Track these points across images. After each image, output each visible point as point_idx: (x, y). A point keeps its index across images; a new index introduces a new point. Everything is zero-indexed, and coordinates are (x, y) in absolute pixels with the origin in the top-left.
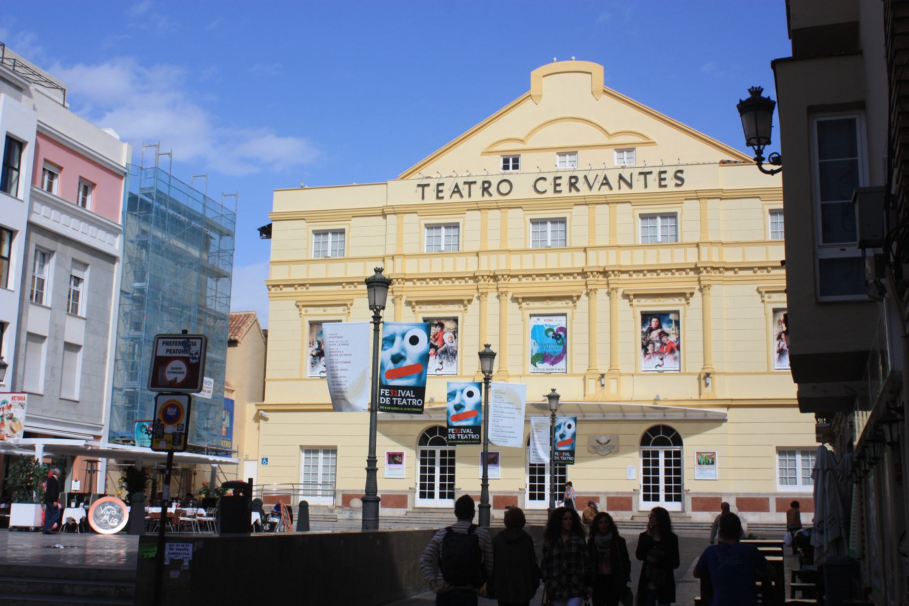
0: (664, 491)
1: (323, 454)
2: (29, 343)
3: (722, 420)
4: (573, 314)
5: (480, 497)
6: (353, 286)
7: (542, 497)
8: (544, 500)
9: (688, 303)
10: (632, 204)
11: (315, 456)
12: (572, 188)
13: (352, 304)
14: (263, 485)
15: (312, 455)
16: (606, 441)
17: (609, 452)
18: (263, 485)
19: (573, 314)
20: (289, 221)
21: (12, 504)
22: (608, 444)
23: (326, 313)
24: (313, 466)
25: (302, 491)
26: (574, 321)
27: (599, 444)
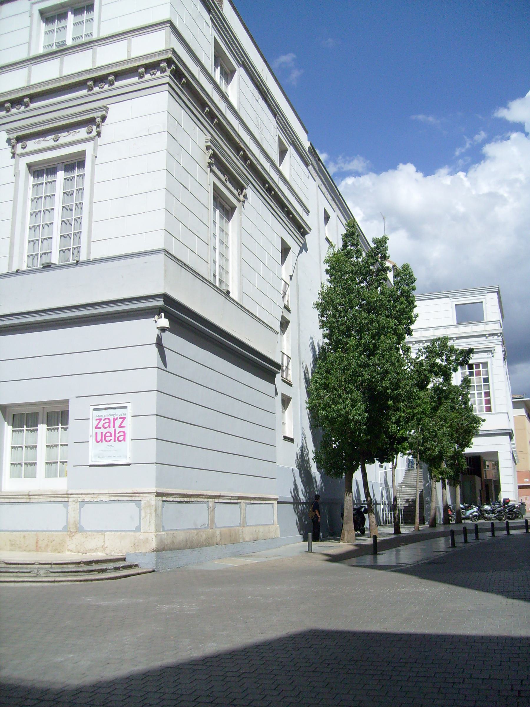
1: (63, 172)
2: (485, 320)
4: (492, 362)
5: (506, 528)
6: (491, 353)
11: (50, 178)
13: (104, 118)
15: (44, 179)
19: (492, 362)
20: (19, 121)
21: (292, 505)
23: (58, 143)
24: (61, 445)
26: (97, 161)
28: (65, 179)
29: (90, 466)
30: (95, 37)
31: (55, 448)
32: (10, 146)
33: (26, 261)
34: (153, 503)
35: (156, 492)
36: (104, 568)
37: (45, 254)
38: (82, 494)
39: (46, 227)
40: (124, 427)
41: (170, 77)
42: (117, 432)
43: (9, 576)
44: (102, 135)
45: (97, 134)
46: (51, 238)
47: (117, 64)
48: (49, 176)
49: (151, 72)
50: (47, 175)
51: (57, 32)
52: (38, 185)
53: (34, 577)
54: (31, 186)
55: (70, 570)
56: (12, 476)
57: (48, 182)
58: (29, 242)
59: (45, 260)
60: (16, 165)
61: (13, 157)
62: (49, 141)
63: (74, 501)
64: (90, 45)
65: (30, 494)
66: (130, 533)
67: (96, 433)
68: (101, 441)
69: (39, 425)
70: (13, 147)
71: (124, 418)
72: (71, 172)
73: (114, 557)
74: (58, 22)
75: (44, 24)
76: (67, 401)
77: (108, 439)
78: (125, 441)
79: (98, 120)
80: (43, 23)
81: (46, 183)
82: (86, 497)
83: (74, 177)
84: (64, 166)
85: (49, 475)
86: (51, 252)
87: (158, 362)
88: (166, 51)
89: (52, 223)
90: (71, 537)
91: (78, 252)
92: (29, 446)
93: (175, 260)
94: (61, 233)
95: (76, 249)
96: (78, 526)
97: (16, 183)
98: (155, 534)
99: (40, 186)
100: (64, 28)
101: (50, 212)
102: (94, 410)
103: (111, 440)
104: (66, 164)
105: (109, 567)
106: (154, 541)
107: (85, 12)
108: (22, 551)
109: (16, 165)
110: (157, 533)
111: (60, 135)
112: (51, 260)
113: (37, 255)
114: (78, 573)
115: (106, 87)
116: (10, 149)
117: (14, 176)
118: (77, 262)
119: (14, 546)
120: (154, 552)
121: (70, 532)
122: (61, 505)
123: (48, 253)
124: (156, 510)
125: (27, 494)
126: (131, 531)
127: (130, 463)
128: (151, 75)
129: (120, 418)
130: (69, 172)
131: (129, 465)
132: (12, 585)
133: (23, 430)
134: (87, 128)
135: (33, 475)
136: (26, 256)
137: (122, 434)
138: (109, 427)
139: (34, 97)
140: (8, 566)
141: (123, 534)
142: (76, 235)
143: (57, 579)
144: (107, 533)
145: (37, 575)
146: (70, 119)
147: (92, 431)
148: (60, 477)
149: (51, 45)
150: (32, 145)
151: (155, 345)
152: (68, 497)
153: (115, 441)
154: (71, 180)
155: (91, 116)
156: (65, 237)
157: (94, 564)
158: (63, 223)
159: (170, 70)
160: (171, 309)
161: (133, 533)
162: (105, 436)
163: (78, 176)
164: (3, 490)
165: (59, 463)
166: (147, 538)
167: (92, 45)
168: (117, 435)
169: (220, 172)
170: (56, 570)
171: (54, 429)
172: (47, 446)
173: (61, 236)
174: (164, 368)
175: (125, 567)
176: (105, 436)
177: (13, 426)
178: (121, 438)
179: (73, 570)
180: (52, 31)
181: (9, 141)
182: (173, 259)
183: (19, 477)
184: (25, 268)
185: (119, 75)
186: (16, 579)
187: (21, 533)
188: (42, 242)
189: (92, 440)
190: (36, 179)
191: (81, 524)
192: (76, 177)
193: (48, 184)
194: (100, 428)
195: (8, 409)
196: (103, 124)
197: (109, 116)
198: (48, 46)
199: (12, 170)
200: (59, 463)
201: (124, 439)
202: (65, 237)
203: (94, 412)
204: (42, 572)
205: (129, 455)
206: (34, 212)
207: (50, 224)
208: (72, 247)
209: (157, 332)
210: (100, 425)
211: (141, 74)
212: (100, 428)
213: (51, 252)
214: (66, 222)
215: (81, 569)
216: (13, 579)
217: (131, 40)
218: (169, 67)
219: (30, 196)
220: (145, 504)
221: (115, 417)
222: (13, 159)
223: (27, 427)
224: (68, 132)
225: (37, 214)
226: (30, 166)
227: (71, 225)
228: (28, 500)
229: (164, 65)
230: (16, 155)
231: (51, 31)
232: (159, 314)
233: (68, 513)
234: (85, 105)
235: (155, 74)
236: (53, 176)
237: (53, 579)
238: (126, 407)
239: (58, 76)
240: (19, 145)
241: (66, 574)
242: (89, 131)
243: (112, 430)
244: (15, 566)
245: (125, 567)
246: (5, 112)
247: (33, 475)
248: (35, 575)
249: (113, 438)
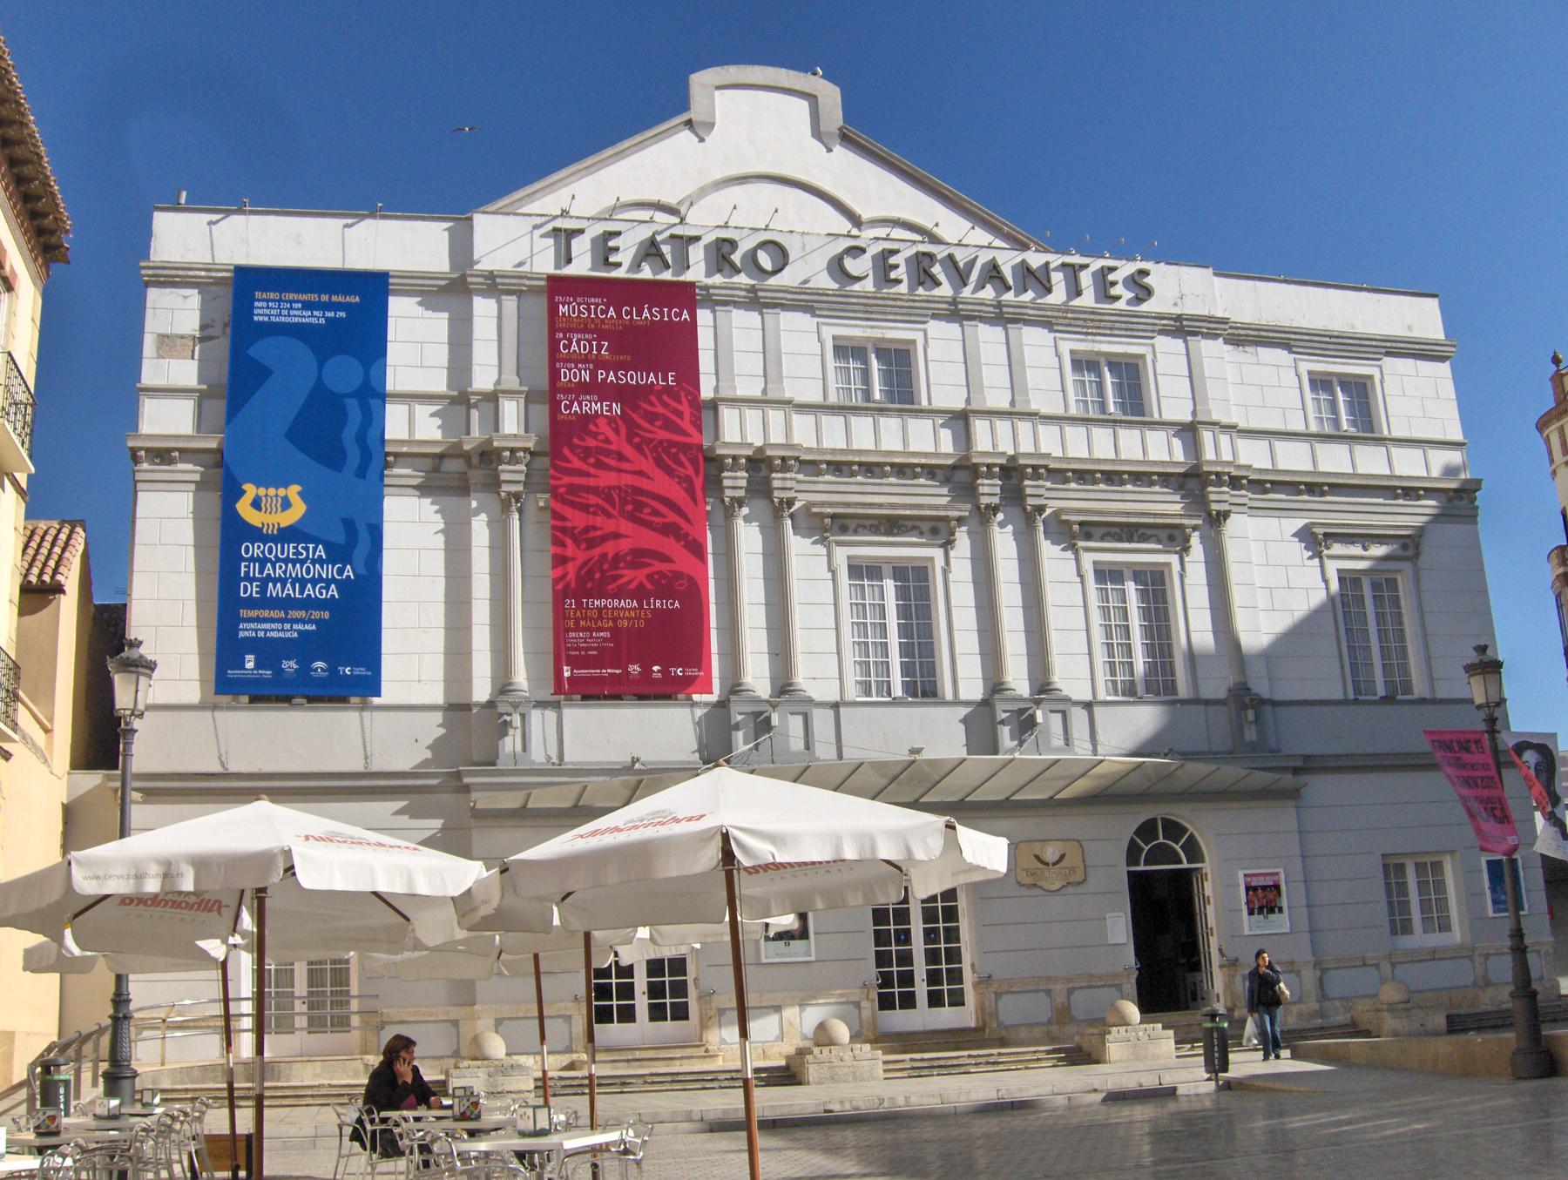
0: (646, 995)
7: (957, 1000)
8: (915, 1007)
16: (1056, 857)
17: (1064, 883)
22: (1058, 866)
27: (1040, 866)
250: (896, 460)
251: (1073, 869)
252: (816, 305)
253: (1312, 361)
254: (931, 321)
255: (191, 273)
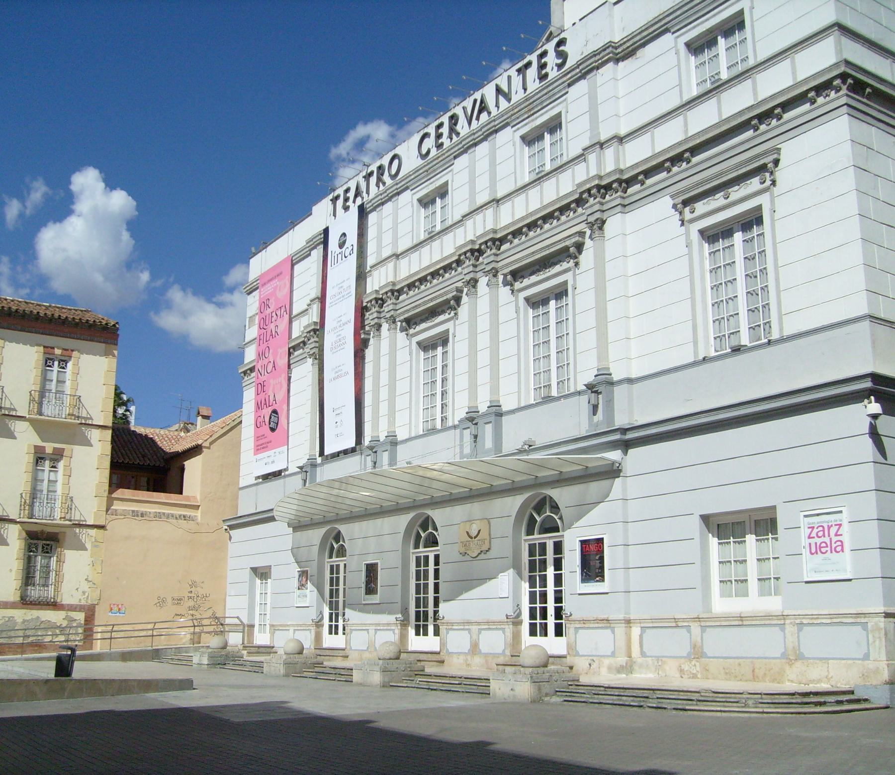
3: (613, 472)
9: (577, 264)
10: (672, 31)
11: (727, 243)
12: (500, 96)
13: (776, 162)
14: (113, 625)
18: (155, 623)
23: (730, 200)
24: (773, 558)
25: (99, 634)
26: (777, 216)
28: (744, 241)
29: (807, 582)
30: (751, 62)
31: (766, 561)
32: (677, 212)
33: (713, 345)
34: (882, 625)
35: (884, 613)
36: (822, 700)
37: (733, 333)
38: (799, 615)
39: (730, 301)
40: (841, 535)
41: (847, 95)
42: (833, 543)
43: (712, 705)
44: (778, 183)
45: (771, 182)
46: (738, 314)
47: (781, 93)
48: (725, 240)
49: (823, 94)
50: (723, 239)
51: (709, 63)
52: (714, 252)
53: (743, 707)
54: (707, 255)
55: (781, 701)
56: (722, 595)
57: (726, 247)
58: (714, 322)
59: (734, 343)
60: (687, 234)
61: (682, 224)
62: (718, 200)
63: (791, 623)
64: (748, 75)
65: (742, 616)
66: (857, 661)
67: (810, 544)
68: (817, 553)
69: (746, 536)
70: (681, 213)
71: (840, 525)
72: (750, 231)
73: (839, 690)
74: (708, 51)
75: (693, 57)
76: (774, 508)
77: (823, 550)
78: (843, 551)
79: (770, 165)
80: (692, 55)
81: (723, 249)
82: (804, 618)
83: (754, 237)
84: (740, 226)
85: (762, 593)
86: (739, 331)
87: (874, 455)
88: (836, 65)
89: (737, 296)
90: (791, 665)
91: (770, 327)
92: (738, 561)
93: (887, 324)
94: (748, 307)
95: (768, 324)
96: (798, 652)
97: (690, 254)
98: (887, 662)
99: (717, 253)
100: (716, 56)
101: (732, 283)
102: (805, 516)
103: (827, 551)
104: (741, 222)
105: (830, 700)
106: (886, 671)
107: (737, 32)
108: (738, 681)
109: (687, 234)
110: (889, 662)
111: (730, 190)
112: (740, 342)
113: (724, 336)
114: (791, 705)
115: (774, 122)
116: (678, 216)
117: (687, 247)
118: (769, 341)
119: (729, 675)
120: (887, 684)
121: (790, 659)
122: (777, 628)
123: (736, 332)
124: (886, 634)
125: (739, 616)
126: (859, 659)
127: (851, 578)
128: (825, 97)
129: (836, 525)
130: (747, 232)
131: (850, 580)
132: (719, 714)
133: (730, 542)
134: (758, 177)
135: (746, 594)
136: (713, 339)
137: (839, 543)
138: (824, 536)
139: (695, 150)
140: (717, 695)
141: (850, 662)
142: (765, 307)
143: (765, 710)
144: (830, 661)
145: (746, 706)
146: (737, 170)
147: (805, 542)
148: (775, 595)
149: (705, 81)
150: (701, 207)
151: (868, 435)
152: (784, 619)
153: (831, 552)
154: (751, 241)
155: (762, 162)
156: (753, 311)
157: (812, 696)
158: (749, 295)
159: (846, 86)
160: (890, 390)
161: (860, 662)
162: (820, 547)
163: (757, 235)
164: (713, 611)
165: (772, 579)
166: (878, 668)
167: (750, 73)
168: (834, 546)
169: (421, 325)
170: (766, 701)
171: (764, 540)
172: (758, 560)
173: (749, 310)
174: (883, 461)
175: (850, 702)
176: (820, 547)
177: (756, 535)
178: (839, 549)
179: (785, 701)
180: (703, 64)
181: (675, 206)
182: (882, 323)
183: (730, 596)
184: (713, 354)
185: (787, 106)
186: (723, 709)
187: (736, 660)
188: (728, 320)
189: (806, 552)
190: (711, 245)
191: (801, 651)
192: (756, 237)
193: (726, 249)
194: (814, 537)
195: (711, 519)
196: (776, 169)
197: (782, 158)
198: (701, 82)
199: (682, 241)
200: (772, 579)
201: (842, 550)
202: (753, 311)
203: (805, 519)
204: (750, 702)
205: (849, 567)
206: (715, 286)
207: (735, 297)
208: (762, 322)
209: (869, 419)
210: (813, 534)
211: (812, 99)
212: (814, 537)
213: (739, 331)
214: (752, 292)
215: (794, 701)
216: (719, 709)
217: (793, 57)
218: (844, 82)
219: (707, 267)
220: (872, 626)
221: (830, 524)
222: (682, 227)
223: (733, 538)
224: (739, 185)
225: (718, 287)
226: (702, 232)
227: (757, 295)
228: (740, 623)
229: (837, 82)
230: (685, 222)
231: (702, 63)
232: (868, 398)
233: (785, 638)
234: (753, 149)
235: (829, 96)
236: (730, 239)
237: (761, 710)
238: (841, 512)
239: (718, 121)
240: (687, 210)
241: (777, 705)
242: (762, 181)
243: (827, 540)
244: (723, 695)
245: (850, 702)
246: (666, 172)
247: (746, 594)
248: (743, 705)
249: (828, 549)
250: (431, 270)
251: (483, 541)
252: (408, 184)
253: (690, 30)
254: (455, 161)
255: (253, 285)
